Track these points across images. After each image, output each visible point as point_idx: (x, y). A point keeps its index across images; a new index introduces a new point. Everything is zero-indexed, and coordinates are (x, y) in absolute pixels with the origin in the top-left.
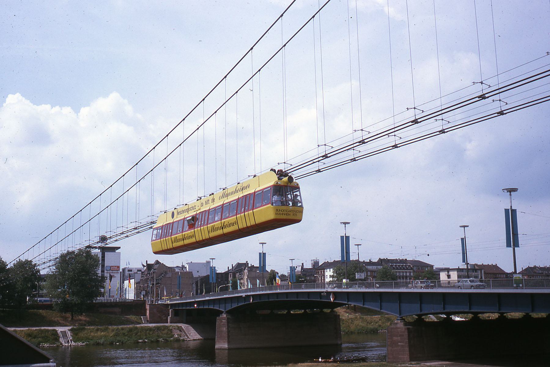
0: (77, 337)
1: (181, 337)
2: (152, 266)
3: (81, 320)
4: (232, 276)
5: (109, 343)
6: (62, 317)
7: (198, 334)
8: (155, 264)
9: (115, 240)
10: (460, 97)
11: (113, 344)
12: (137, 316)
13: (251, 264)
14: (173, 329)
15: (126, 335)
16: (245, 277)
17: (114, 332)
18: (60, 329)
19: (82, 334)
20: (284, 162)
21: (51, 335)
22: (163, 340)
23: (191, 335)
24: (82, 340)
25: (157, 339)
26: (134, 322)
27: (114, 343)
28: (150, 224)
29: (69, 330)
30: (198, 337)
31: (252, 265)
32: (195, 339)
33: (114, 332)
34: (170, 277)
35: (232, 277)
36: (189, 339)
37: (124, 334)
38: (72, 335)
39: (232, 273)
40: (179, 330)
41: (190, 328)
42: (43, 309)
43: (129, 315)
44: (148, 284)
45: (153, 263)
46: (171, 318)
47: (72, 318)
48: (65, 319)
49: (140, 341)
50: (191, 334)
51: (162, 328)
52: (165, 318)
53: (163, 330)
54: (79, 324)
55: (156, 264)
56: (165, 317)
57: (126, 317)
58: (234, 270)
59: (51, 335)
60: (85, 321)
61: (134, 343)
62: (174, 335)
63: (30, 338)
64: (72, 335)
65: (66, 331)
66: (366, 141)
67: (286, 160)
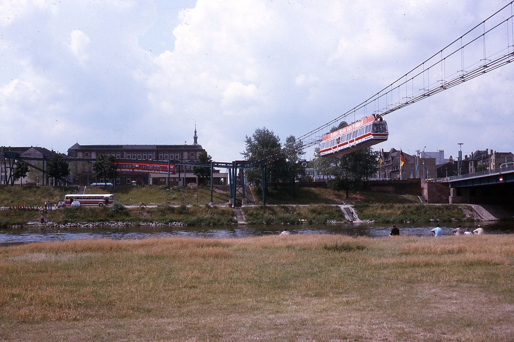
0: (363, 214)
1: (474, 217)
2: (389, 154)
3: (356, 199)
4: (473, 163)
5: (398, 221)
6: (336, 195)
7: (491, 215)
8: (392, 152)
9: (440, 86)
10: (428, 90)
11: (403, 222)
12: (414, 195)
13: (495, 151)
14: (463, 208)
15: (415, 214)
16: (491, 164)
17: (401, 210)
18: (342, 207)
19: (367, 212)
20: (512, 45)
21: (336, 212)
22: (456, 219)
23: (484, 216)
24: (369, 218)
25: (449, 218)
26: (413, 202)
27: (404, 221)
28: (483, 68)
29: (352, 207)
30: (492, 217)
31: (496, 152)
32: (490, 219)
33: (401, 210)
34: (412, 164)
35: (473, 165)
36: (482, 220)
37: (412, 212)
38: (356, 212)
39: (473, 161)
40: (470, 210)
41: (481, 207)
42: (315, 187)
43: (406, 194)
44: (386, 172)
45: (389, 152)
46: (453, 198)
47: (347, 196)
48: (339, 196)
49: (431, 220)
50: (484, 215)
51: (452, 208)
52: (446, 198)
53: (453, 210)
54: (356, 202)
55: (392, 153)
56: (445, 196)
57: (403, 197)
58: (474, 158)
59: (336, 212)
60: (361, 199)
61: (426, 222)
62: (466, 215)
63: (315, 214)
64: (356, 212)
65: (350, 208)
66: (511, 61)
67: (463, 69)
